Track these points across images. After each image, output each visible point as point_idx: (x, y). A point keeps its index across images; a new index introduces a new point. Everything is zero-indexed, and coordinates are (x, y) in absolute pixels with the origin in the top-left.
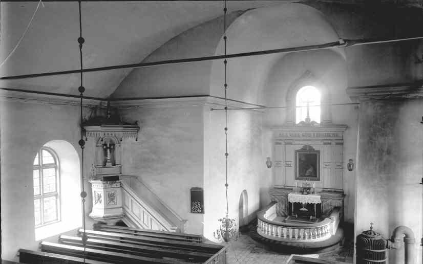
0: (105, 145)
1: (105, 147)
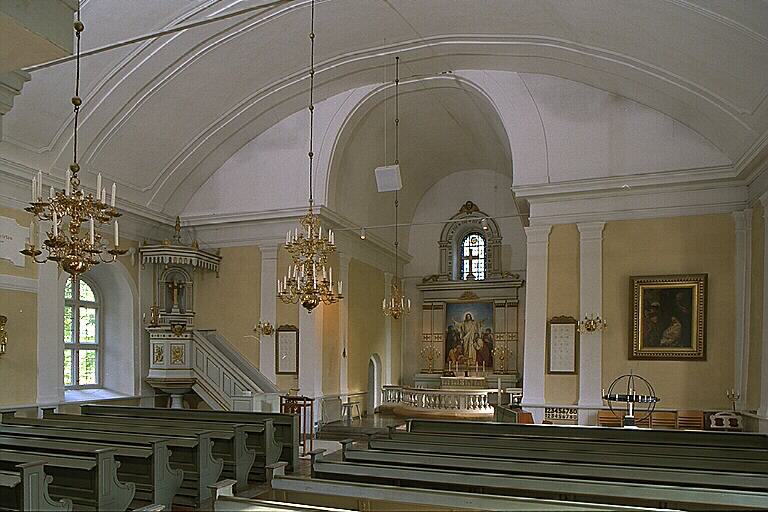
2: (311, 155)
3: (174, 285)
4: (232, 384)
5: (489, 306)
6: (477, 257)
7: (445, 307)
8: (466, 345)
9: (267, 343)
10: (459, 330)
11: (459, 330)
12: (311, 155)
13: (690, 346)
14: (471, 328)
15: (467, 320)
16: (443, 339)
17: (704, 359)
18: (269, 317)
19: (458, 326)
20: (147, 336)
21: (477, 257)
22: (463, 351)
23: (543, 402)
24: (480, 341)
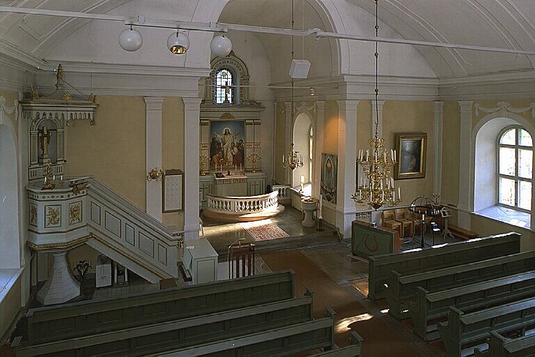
0: (42, 131)
1: (40, 135)
2: (376, 55)
3: (45, 139)
4: (137, 234)
5: (242, 124)
6: (222, 87)
7: (209, 124)
8: (225, 152)
9: (154, 187)
10: (220, 141)
11: (220, 141)
12: (376, 55)
13: (419, 171)
14: (229, 139)
15: (226, 134)
16: (209, 147)
17: (424, 177)
18: (156, 162)
19: (219, 137)
20: (29, 196)
21: (222, 87)
22: (223, 156)
23: (355, 211)
24: (236, 149)
